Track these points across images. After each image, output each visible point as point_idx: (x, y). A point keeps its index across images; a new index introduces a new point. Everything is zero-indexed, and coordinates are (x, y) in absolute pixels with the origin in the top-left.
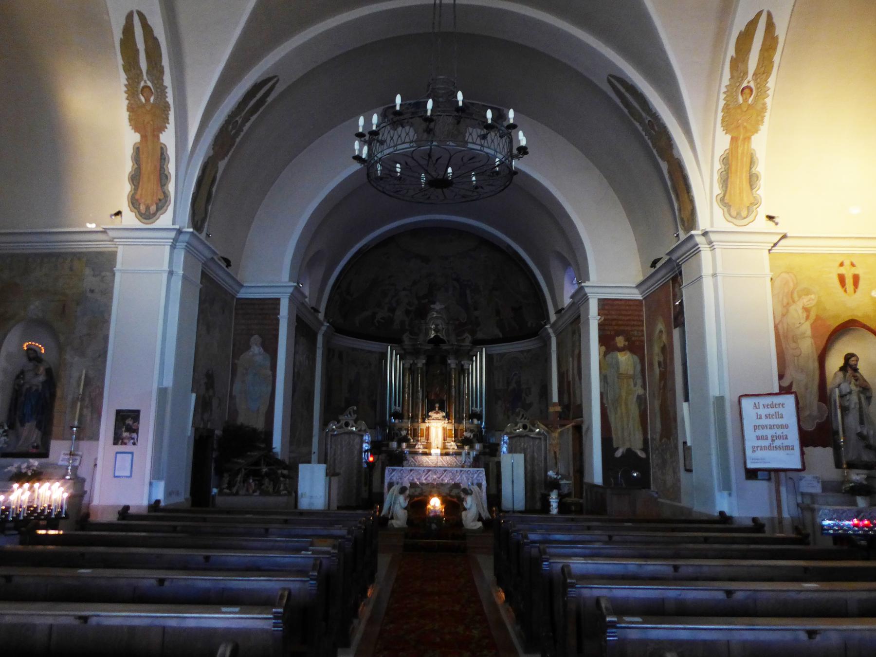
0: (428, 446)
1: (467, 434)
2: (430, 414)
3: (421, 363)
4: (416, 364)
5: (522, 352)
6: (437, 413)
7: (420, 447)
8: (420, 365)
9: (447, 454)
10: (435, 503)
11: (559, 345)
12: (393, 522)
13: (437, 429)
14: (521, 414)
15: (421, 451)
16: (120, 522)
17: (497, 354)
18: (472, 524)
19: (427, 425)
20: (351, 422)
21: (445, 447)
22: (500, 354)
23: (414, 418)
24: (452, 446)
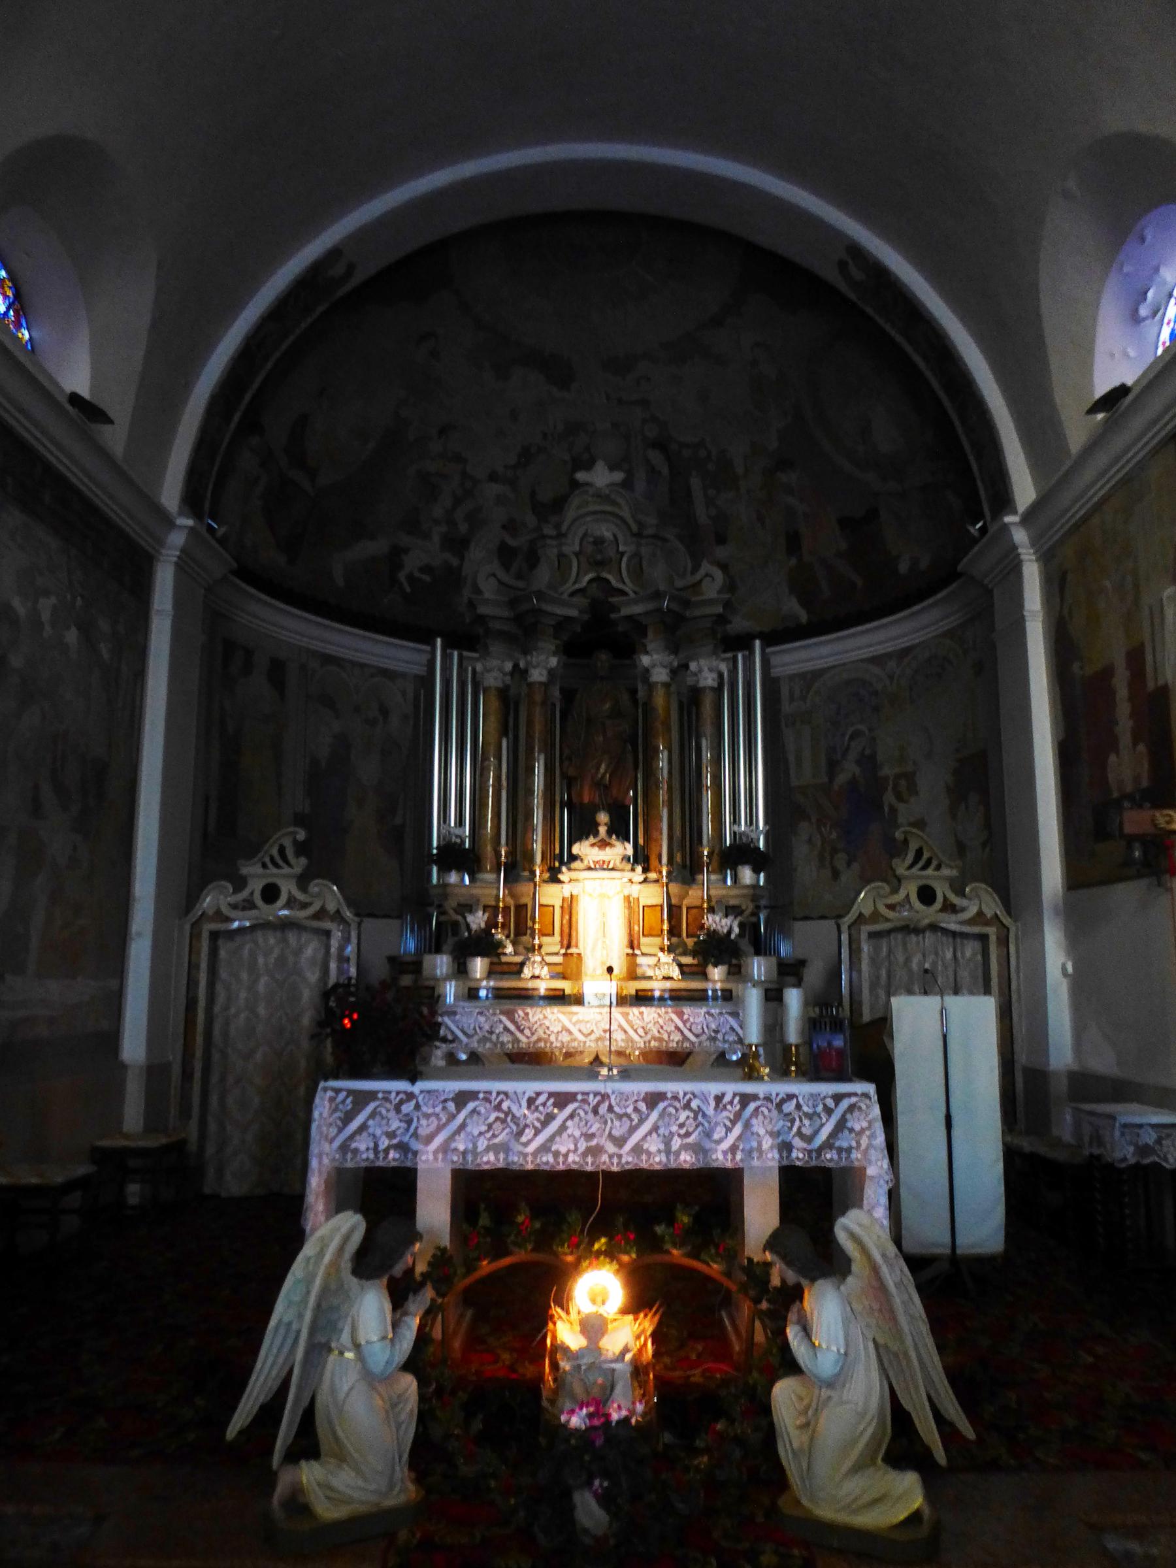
0: (570, 967)
1: (717, 922)
2: (576, 849)
3: (543, 664)
4: (524, 673)
5: (876, 660)
6: (603, 844)
7: (538, 975)
8: (538, 675)
9: (642, 999)
10: (598, 1309)
11: (1057, 585)
12: (309, 1474)
13: (603, 901)
14: (913, 846)
15: (542, 987)
16: (512, 1007)
17: (792, 678)
18: (853, 1487)
19: (566, 890)
20: (288, 888)
21: (633, 974)
22: (802, 676)
23: (516, 867)
24: (662, 968)
